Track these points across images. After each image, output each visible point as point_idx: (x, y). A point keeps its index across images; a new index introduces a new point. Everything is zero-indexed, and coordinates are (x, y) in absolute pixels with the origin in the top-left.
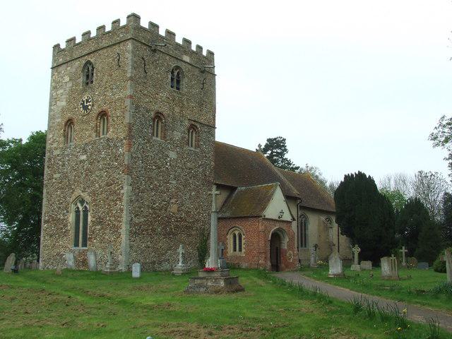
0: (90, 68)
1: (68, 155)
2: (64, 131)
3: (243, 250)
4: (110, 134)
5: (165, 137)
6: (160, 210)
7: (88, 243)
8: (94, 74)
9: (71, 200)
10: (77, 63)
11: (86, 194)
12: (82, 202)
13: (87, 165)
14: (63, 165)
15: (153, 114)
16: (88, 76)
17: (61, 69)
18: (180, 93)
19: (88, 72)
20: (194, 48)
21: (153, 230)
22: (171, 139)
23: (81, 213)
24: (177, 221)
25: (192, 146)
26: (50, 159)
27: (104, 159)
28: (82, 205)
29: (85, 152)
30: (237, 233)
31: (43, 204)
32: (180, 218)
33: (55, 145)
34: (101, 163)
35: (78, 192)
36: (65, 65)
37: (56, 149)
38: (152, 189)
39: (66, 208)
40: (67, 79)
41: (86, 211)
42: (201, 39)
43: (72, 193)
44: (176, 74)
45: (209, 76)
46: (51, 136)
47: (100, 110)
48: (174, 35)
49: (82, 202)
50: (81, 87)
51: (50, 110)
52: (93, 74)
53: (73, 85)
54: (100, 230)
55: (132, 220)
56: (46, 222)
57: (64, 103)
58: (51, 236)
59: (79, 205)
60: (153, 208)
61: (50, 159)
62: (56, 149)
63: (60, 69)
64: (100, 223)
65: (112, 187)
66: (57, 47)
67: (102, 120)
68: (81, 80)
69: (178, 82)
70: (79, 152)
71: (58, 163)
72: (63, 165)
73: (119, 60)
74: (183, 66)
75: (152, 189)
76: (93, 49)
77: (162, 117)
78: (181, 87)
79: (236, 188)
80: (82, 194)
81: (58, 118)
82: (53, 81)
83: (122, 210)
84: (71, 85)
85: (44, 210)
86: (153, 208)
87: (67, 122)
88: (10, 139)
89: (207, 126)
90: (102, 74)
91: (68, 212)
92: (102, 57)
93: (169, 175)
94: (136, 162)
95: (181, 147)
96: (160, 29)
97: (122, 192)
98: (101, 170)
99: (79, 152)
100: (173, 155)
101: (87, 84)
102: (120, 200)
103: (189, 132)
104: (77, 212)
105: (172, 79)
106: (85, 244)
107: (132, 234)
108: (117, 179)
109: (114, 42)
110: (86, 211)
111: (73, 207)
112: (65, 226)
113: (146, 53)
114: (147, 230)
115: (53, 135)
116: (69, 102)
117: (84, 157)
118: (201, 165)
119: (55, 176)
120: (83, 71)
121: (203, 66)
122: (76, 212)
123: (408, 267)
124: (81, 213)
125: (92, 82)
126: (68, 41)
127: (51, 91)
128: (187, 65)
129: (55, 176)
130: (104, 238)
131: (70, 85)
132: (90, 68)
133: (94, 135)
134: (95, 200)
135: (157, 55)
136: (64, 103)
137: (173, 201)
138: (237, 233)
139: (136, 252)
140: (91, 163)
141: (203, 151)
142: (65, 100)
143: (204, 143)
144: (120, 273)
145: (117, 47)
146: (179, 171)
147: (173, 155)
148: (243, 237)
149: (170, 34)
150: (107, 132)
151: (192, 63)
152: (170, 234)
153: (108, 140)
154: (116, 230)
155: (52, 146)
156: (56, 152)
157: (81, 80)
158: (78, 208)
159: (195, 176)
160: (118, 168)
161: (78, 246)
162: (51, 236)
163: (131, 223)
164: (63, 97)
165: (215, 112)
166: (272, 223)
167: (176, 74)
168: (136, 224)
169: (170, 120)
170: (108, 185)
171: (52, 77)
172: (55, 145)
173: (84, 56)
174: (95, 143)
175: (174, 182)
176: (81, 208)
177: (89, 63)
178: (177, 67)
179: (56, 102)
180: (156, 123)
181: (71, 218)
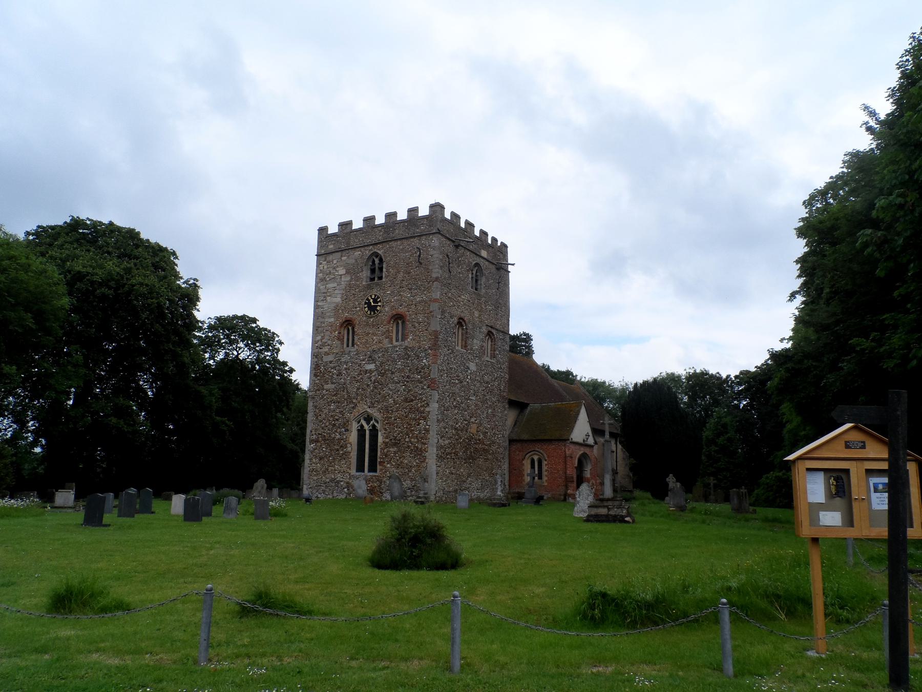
0: (377, 261)
1: (346, 363)
3: (545, 478)
4: (409, 342)
5: (466, 346)
6: (462, 430)
7: (379, 467)
8: (384, 270)
10: (357, 253)
12: (368, 419)
14: (339, 374)
15: (455, 320)
16: (373, 271)
17: (335, 258)
19: (376, 268)
20: (477, 233)
21: (456, 454)
22: (471, 349)
23: (367, 432)
24: (475, 444)
27: (401, 371)
28: (368, 423)
29: (371, 359)
30: (536, 458)
32: (479, 440)
33: (326, 349)
34: (397, 374)
35: (363, 407)
36: (339, 254)
37: (327, 354)
38: (455, 407)
40: (342, 271)
42: (497, 231)
43: (353, 408)
45: (502, 271)
47: (394, 313)
49: (368, 419)
51: (316, 307)
52: (381, 269)
54: (395, 453)
56: (312, 441)
57: (338, 300)
58: (321, 459)
60: (456, 429)
62: (327, 354)
63: (330, 257)
64: (395, 445)
66: (322, 230)
67: (395, 324)
68: (366, 273)
69: (477, 281)
72: (339, 374)
73: (419, 256)
74: (481, 262)
75: (455, 407)
77: (463, 323)
78: (479, 287)
79: (527, 405)
80: (368, 410)
81: (329, 317)
82: (319, 271)
84: (348, 278)
86: (456, 429)
87: (344, 322)
89: (502, 332)
91: (347, 430)
93: (469, 389)
94: (442, 376)
95: (480, 358)
96: (475, 229)
97: (427, 409)
99: (363, 360)
100: (473, 367)
104: (361, 432)
106: (373, 468)
107: (440, 458)
108: (420, 395)
110: (374, 432)
111: (355, 427)
113: (450, 248)
116: (346, 299)
119: (326, 387)
123: (480, 503)
124: (367, 432)
125: (380, 278)
126: (342, 225)
127: (317, 283)
128: (484, 261)
129: (326, 387)
130: (401, 462)
132: (377, 261)
135: (461, 251)
136: (338, 300)
137: (473, 420)
138: (536, 458)
139: (441, 479)
141: (498, 361)
142: (339, 296)
143: (500, 352)
145: (416, 240)
146: (478, 385)
147: (473, 367)
148: (544, 463)
149: (470, 225)
151: (490, 259)
152: (469, 459)
153: (406, 348)
154: (419, 453)
156: (330, 358)
158: (362, 426)
159: (491, 392)
161: (363, 471)
162: (321, 459)
163: (440, 447)
166: (577, 447)
168: (442, 447)
169: (470, 326)
170: (406, 400)
171: (317, 266)
175: (474, 398)
176: (366, 427)
177: (376, 255)
178: (477, 265)
179: (325, 297)
181: (353, 437)
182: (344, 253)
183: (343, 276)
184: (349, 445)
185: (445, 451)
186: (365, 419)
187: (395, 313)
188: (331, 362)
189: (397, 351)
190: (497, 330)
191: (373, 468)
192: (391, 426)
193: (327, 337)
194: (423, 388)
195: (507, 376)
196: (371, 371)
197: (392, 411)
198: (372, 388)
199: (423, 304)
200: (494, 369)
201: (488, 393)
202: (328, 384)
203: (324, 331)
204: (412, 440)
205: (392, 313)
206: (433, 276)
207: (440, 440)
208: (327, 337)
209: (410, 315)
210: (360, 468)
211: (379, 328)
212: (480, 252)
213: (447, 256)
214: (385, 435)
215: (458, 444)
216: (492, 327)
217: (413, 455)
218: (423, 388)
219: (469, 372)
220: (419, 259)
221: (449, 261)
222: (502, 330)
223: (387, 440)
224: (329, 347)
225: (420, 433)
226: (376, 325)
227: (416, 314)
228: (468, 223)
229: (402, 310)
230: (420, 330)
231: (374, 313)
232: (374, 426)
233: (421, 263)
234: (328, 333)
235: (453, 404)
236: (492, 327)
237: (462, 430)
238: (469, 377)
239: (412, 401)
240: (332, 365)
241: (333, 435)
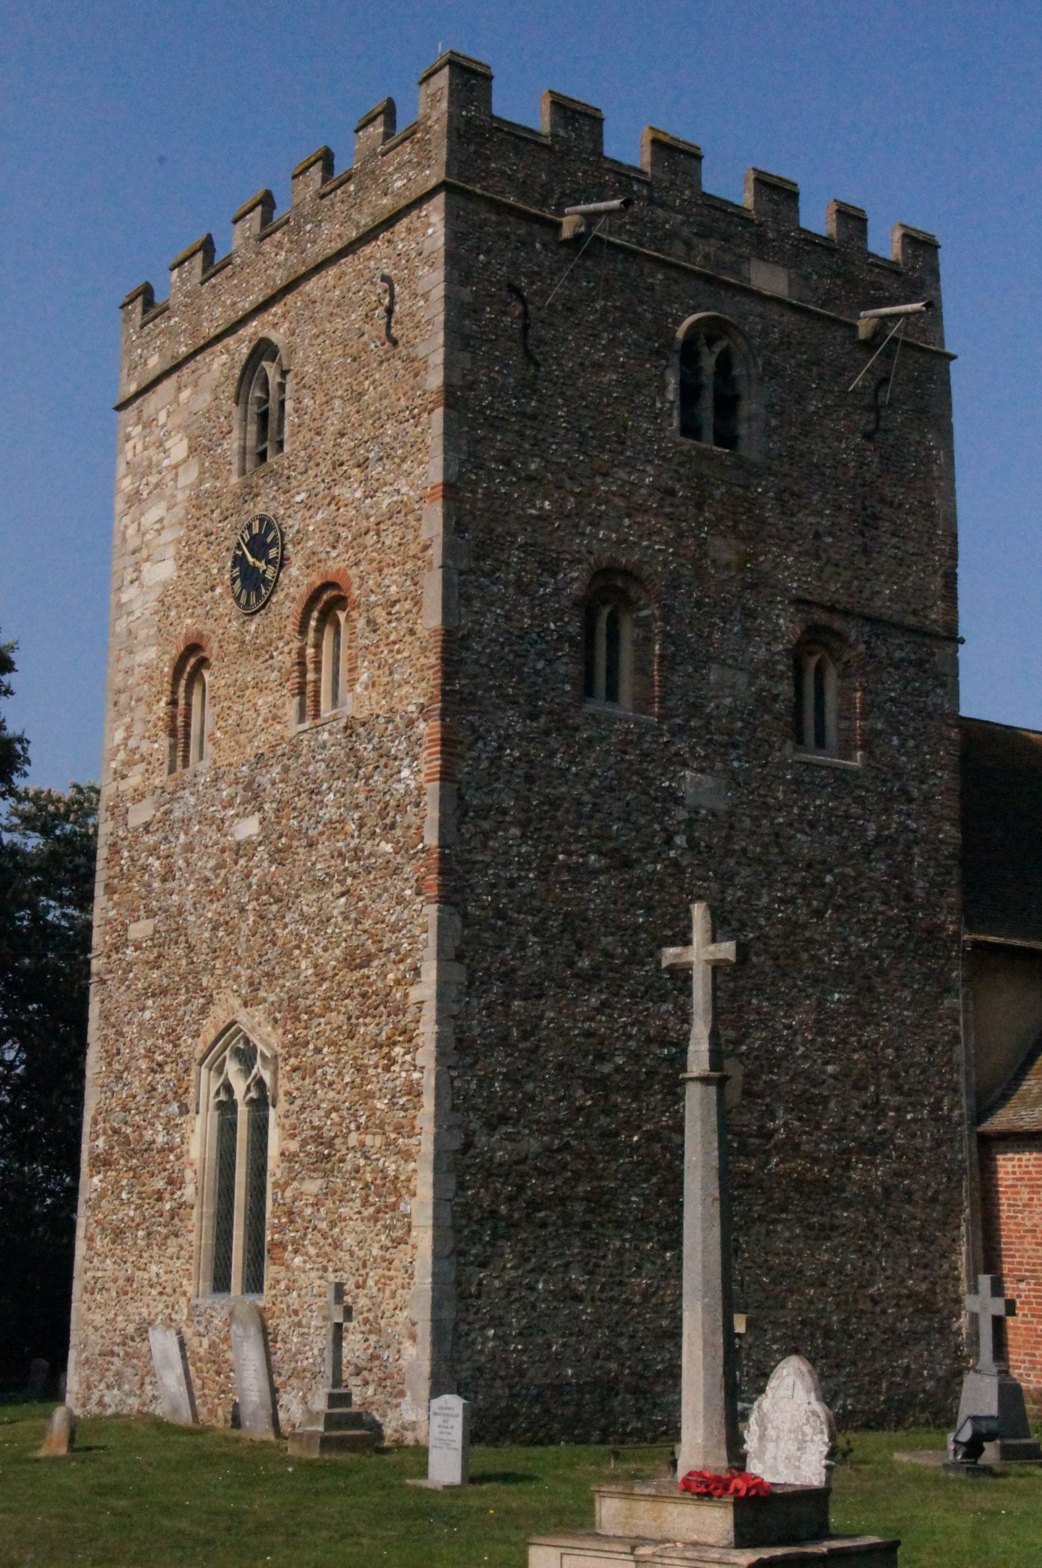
1: (185, 822)
2: (173, 703)
6: (637, 1091)
8: (289, 406)
9: (200, 1048)
11: (259, 1013)
12: (247, 1057)
13: (262, 867)
18: (741, 464)
22: (695, 708)
23: (243, 1113)
25: (820, 742)
26: (114, 849)
27: (335, 827)
31: (89, 1073)
33: (135, 779)
34: (322, 849)
36: (168, 385)
37: (139, 796)
39: (179, 1093)
40: (178, 448)
41: (260, 1104)
43: (203, 1011)
44: (708, 363)
46: (119, 735)
47: (316, 579)
48: (694, 156)
49: (247, 1057)
50: (234, 479)
52: (282, 404)
53: (202, 473)
55: (468, 1145)
56: (103, 1162)
59: (232, 1068)
60: (594, 1082)
61: (114, 849)
62: (139, 796)
65: (372, 971)
70: (229, 804)
71: (145, 868)
73: (390, 311)
76: (280, 278)
80: (242, 1016)
83: (414, 1091)
85: (92, 1100)
86: (594, 1082)
87: (183, 658)
88: (55, 795)
90: (320, 398)
92: (322, 310)
98: (322, 884)
99: (229, 804)
101: (262, 456)
102: (408, 1035)
103: (798, 669)
104: (227, 1108)
105: (689, 393)
108: (395, 929)
109: (365, 220)
110: (260, 1104)
112: (175, 1182)
114: (563, 1200)
115: (128, 728)
116: (187, 560)
117: (248, 828)
118: (878, 842)
120: (239, 398)
121: (694, 156)
122: (220, 1105)
124: (243, 1113)
125: (280, 445)
128: (774, 313)
131: (189, 475)
133: (291, 708)
134: (297, 1043)
140: (279, 856)
142: (171, 551)
144: (851, 1412)
145: (377, 248)
150: (352, 682)
155: (124, 785)
156: (141, 814)
157: (232, 444)
158: (228, 1088)
160: (397, 871)
164: (168, 536)
165: (954, 556)
167: (708, 363)
168: (489, 1172)
170: (357, 960)
172: (135, 779)
173: (243, 321)
174: (295, 752)
176: (239, 1087)
177: (264, 350)
180: (602, 625)
182: (186, 371)
183: (180, 470)
184: (189, 1174)
185: (521, 1189)
186: (237, 1053)
187: (318, 583)
188: (147, 827)
189: (324, 746)
190: (872, 620)
191: (254, 1283)
192: (307, 1080)
193: (138, 729)
194: (400, 900)
195: (949, 832)
196: (240, 850)
197: (308, 1010)
198: (251, 919)
199: (401, 517)
200: (860, 801)
201: (819, 914)
202: (138, 919)
203: (133, 703)
204: (369, 1140)
205: (309, 585)
206: (427, 387)
207: (482, 1140)
208: (138, 729)
209: (361, 578)
210: (221, 1283)
211: (272, 657)
212: (738, 273)
213: (515, 290)
214: (287, 1122)
215: (614, 1153)
216: (831, 609)
217: (372, 1210)
218: (400, 900)
219: (682, 814)
220: (388, 327)
221: (525, 314)
222: (911, 620)
223: (293, 1146)
224: (143, 766)
225: (392, 1104)
226: (263, 650)
227: (380, 571)
228: (766, 184)
229: (336, 563)
230: (392, 637)
231: (259, 597)
232: (260, 1083)
233: (395, 343)
234: (142, 708)
235: (571, 964)
236: (831, 609)
237: (637, 1091)
238: (680, 840)
239: (366, 963)
240: (150, 840)
241: (148, 1134)
